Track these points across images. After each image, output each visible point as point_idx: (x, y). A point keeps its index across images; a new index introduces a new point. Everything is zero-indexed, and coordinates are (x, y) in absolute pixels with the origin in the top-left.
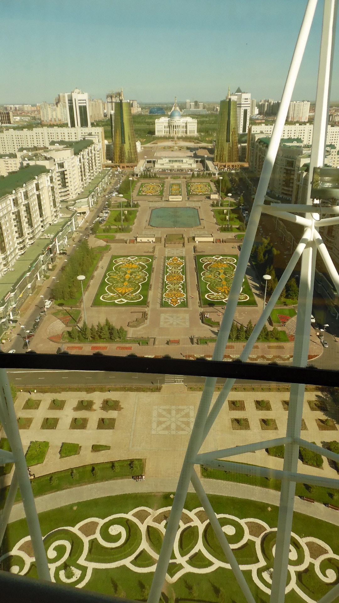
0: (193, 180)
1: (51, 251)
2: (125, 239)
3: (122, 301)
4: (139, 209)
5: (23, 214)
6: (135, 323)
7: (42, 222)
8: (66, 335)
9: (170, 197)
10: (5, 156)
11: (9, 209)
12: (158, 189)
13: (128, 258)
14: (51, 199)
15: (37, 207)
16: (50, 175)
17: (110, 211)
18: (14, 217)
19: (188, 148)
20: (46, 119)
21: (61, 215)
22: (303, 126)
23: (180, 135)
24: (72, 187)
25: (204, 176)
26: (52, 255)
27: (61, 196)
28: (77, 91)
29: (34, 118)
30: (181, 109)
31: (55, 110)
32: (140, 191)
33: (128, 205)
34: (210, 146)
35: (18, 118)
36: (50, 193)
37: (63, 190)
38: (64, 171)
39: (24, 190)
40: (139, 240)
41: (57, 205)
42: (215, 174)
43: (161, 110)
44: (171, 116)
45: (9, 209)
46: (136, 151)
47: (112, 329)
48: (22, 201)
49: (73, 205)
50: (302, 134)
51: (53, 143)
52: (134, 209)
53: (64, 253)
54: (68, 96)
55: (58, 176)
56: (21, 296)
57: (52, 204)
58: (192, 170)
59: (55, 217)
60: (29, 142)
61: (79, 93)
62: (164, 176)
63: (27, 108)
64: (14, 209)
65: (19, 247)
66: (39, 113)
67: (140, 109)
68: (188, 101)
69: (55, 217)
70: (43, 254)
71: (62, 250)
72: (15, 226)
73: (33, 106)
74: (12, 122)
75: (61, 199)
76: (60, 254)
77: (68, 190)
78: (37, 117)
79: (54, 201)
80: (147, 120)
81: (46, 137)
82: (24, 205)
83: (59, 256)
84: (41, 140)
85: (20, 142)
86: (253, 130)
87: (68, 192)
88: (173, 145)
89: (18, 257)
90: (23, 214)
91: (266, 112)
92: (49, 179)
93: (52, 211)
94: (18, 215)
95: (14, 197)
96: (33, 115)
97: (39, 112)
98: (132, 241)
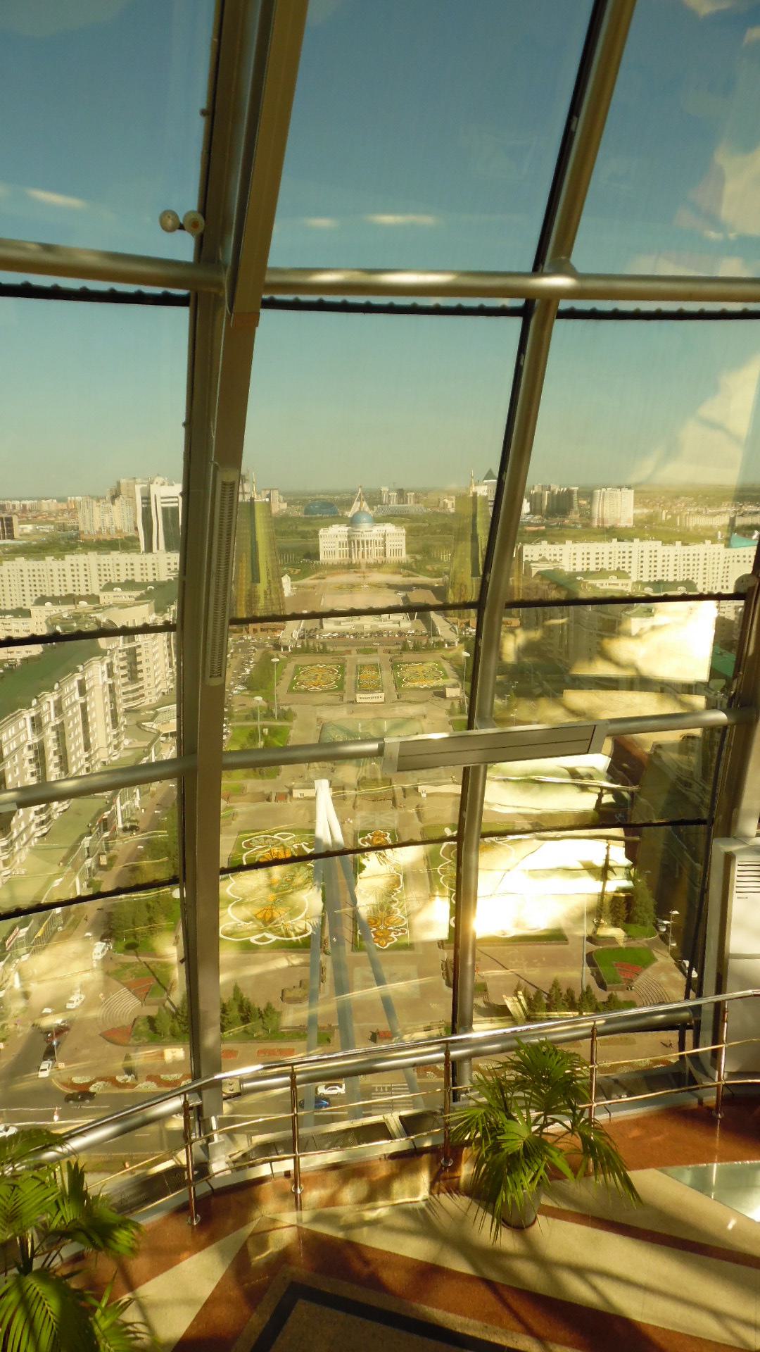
0: (407, 656)
1: (106, 825)
2: (267, 791)
3: (264, 939)
5: (51, 746)
6: (298, 993)
7: (87, 759)
8: (144, 1028)
9: (358, 696)
11: (23, 738)
12: (332, 677)
13: (275, 836)
14: (108, 709)
15: (80, 729)
16: (107, 660)
17: (232, 728)
18: (31, 755)
19: (390, 586)
20: (88, 527)
21: (126, 742)
22: (625, 546)
23: (371, 560)
25: (428, 648)
26: (107, 834)
27: (127, 701)
28: (159, 480)
29: (63, 527)
31: (109, 511)
32: (293, 683)
33: (269, 715)
34: (436, 582)
35: (29, 528)
37: (130, 688)
38: (134, 649)
39: (56, 698)
40: (296, 794)
41: (121, 719)
43: (330, 508)
44: (352, 522)
45: (23, 738)
48: (50, 719)
50: (627, 560)
51: (109, 587)
53: (133, 828)
54: (142, 490)
55: (122, 659)
56: (39, 934)
57: (109, 719)
58: (401, 633)
59: (116, 747)
60: (56, 583)
61: (163, 484)
63: (48, 505)
64: (33, 739)
65: (38, 821)
66: (74, 517)
67: (284, 506)
68: (385, 489)
69: (116, 747)
70: (90, 834)
71: (130, 821)
72: (33, 774)
73: (60, 500)
74: (16, 535)
75: (125, 706)
76: (125, 829)
77: (142, 687)
78: (70, 523)
79: (114, 715)
80: (300, 529)
82: (53, 729)
83: (122, 835)
84: (82, 578)
85: (37, 578)
86: (525, 553)
87: (141, 692)
88: (358, 580)
89: (34, 842)
90: (51, 746)
92: (105, 668)
93: (107, 735)
94: (40, 751)
95: (33, 714)
96: (60, 520)
97: (73, 512)
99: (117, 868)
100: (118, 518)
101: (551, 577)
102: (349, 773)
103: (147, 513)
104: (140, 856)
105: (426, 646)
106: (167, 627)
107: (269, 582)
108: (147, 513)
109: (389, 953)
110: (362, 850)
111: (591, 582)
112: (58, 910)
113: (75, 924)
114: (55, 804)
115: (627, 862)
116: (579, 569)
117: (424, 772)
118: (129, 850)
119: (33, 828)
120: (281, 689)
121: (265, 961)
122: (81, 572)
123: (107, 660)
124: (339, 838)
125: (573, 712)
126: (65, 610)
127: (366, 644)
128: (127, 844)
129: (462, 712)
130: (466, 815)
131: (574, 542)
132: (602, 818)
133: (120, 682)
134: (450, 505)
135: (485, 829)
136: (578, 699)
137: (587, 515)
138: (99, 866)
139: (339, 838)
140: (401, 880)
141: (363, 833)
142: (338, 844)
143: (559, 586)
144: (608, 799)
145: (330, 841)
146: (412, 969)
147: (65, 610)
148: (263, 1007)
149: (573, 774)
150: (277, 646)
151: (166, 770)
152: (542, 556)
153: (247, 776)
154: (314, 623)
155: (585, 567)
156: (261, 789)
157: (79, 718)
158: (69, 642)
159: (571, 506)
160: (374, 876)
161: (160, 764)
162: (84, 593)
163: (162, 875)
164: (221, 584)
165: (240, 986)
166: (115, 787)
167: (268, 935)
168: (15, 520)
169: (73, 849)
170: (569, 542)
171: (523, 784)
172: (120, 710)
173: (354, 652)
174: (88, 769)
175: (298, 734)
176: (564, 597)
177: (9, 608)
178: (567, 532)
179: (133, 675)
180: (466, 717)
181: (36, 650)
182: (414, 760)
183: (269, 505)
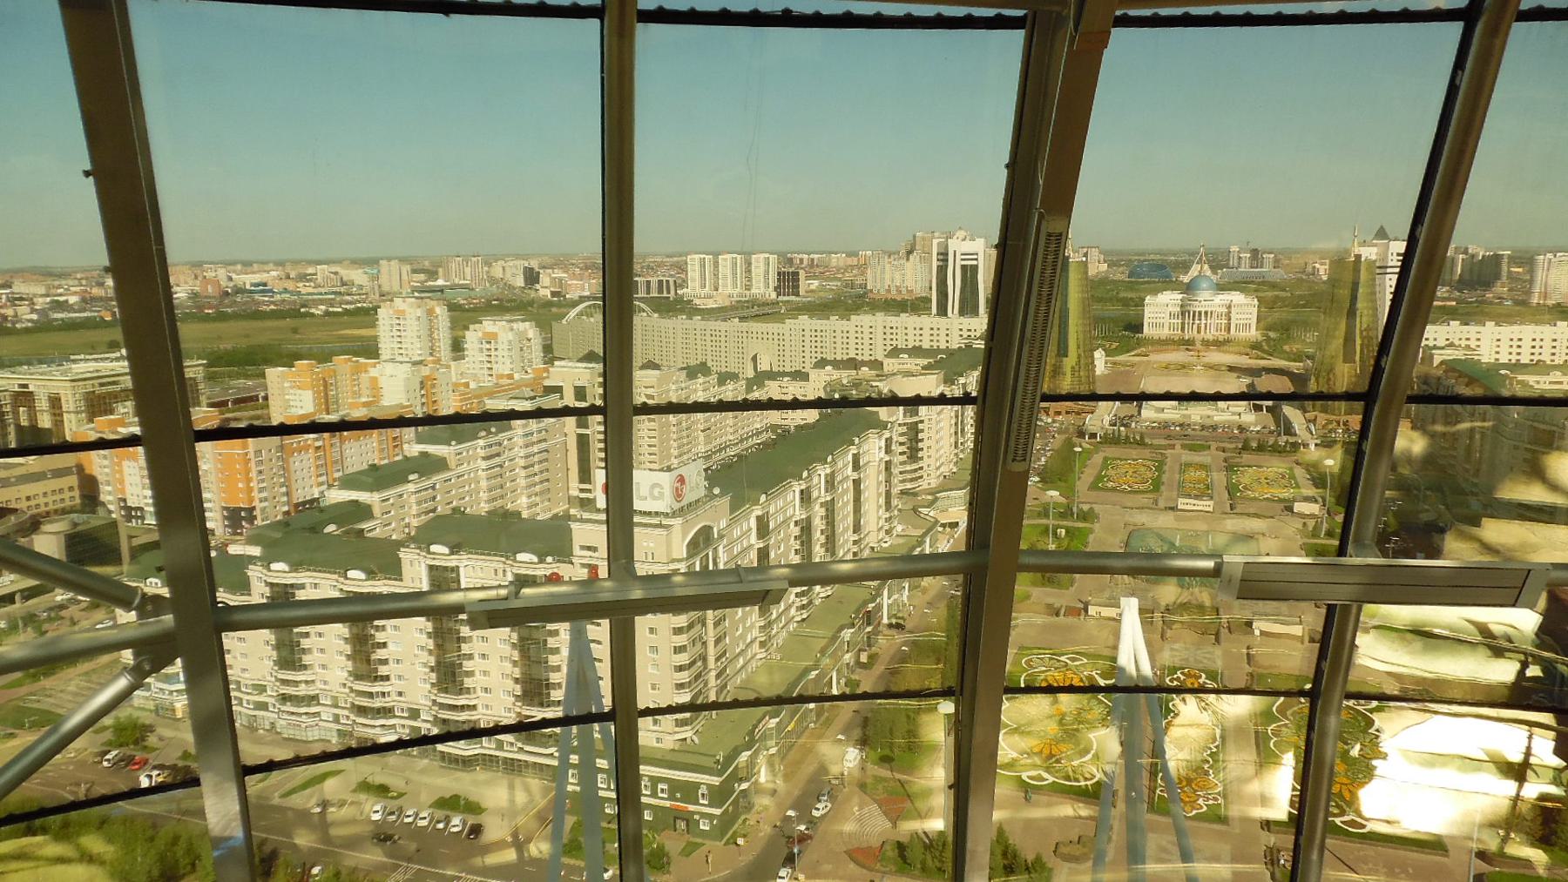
1: (869, 618)
4: (1097, 526)
5: (818, 524)
6: (1077, 850)
7: (855, 542)
8: (891, 853)
10: (784, 374)
14: (883, 489)
15: (850, 508)
16: (887, 434)
18: (796, 531)
19: (1231, 369)
21: (899, 528)
24: (932, 461)
25: (1277, 450)
26: (869, 629)
27: (903, 481)
28: (961, 234)
30: (1214, 269)
32: (1099, 478)
33: (1066, 513)
34: (1296, 367)
35: (815, 284)
36: (882, 477)
37: (908, 468)
39: (828, 471)
40: (1092, 610)
41: (895, 502)
42: (1306, 446)
43: (1162, 272)
44: (1189, 288)
46: (1158, 752)
47: (1015, 856)
48: (820, 494)
49: (930, 505)
51: (895, 352)
52: (1081, 525)
53: (899, 627)
55: (902, 435)
57: (882, 501)
58: (1241, 428)
59: (887, 532)
62: (1163, 442)
63: (837, 260)
64: (800, 514)
68: (1234, 249)
69: (887, 532)
70: (853, 625)
71: (895, 616)
76: (890, 626)
79: (888, 495)
80: (1122, 295)
81: (880, 336)
82: (822, 505)
83: (887, 631)
90: (818, 524)
91: (1461, 280)
92: (883, 443)
94: (806, 528)
96: (848, 276)
97: (862, 268)
98: (1072, 612)
99: (879, 668)
100: (914, 277)
101: (1463, 370)
102: (1169, 592)
103: (942, 270)
104: (904, 658)
105: (1281, 444)
106: (965, 400)
107: (1079, 357)
108: (942, 270)
109: (1195, 824)
110: (1179, 690)
111: (1520, 378)
112: (812, 706)
113: (828, 723)
114: (818, 588)
115: (1558, 762)
116: (1504, 359)
117: (1261, 603)
118: (892, 652)
119: (793, 611)
120: (1083, 483)
121: (1049, 805)
122: (865, 334)
123: (887, 434)
124: (1147, 670)
125: (1488, 548)
126: (845, 376)
127: (1197, 438)
128: (887, 643)
129: (1330, 534)
130: (1326, 666)
131: (1497, 324)
132: (1518, 696)
133: (898, 459)
134: (1323, 271)
135: (1352, 688)
136: (1497, 531)
137: (1523, 287)
138: (859, 663)
139: (1147, 670)
140: (1227, 735)
141: (1173, 670)
142: (1145, 678)
143: (1471, 381)
144: (1534, 671)
145: (1134, 673)
146: (1225, 849)
147: (845, 376)
148: (1030, 858)
149: (1484, 630)
150: (1081, 434)
151: (953, 563)
152: (1445, 340)
153: (1034, 584)
154: (1130, 408)
155: (1514, 358)
156: (1050, 600)
157: (850, 495)
158: (848, 410)
159: (1497, 276)
160: (1191, 725)
161: (935, 556)
162: (866, 358)
163: (935, 684)
164: (1036, 352)
165: (1005, 828)
166: (883, 577)
167: (1045, 775)
168: (802, 274)
169: (834, 638)
170: (1490, 324)
171: (1409, 636)
172: (895, 491)
173: (1178, 447)
174: (855, 554)
175: (1104, 537)
176: (1476, 392)
177: (788, 370)
178: (1487, 309)
179: (913, 453)
180: (1337, 543)
181: (812, 415)
182: (1259, 586)
183: (1085, 264)
